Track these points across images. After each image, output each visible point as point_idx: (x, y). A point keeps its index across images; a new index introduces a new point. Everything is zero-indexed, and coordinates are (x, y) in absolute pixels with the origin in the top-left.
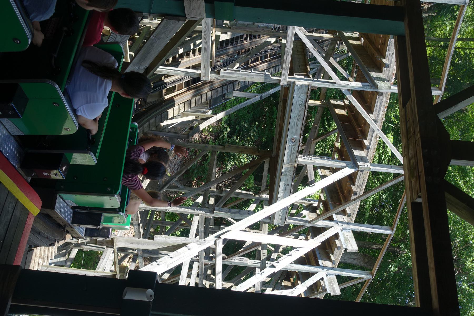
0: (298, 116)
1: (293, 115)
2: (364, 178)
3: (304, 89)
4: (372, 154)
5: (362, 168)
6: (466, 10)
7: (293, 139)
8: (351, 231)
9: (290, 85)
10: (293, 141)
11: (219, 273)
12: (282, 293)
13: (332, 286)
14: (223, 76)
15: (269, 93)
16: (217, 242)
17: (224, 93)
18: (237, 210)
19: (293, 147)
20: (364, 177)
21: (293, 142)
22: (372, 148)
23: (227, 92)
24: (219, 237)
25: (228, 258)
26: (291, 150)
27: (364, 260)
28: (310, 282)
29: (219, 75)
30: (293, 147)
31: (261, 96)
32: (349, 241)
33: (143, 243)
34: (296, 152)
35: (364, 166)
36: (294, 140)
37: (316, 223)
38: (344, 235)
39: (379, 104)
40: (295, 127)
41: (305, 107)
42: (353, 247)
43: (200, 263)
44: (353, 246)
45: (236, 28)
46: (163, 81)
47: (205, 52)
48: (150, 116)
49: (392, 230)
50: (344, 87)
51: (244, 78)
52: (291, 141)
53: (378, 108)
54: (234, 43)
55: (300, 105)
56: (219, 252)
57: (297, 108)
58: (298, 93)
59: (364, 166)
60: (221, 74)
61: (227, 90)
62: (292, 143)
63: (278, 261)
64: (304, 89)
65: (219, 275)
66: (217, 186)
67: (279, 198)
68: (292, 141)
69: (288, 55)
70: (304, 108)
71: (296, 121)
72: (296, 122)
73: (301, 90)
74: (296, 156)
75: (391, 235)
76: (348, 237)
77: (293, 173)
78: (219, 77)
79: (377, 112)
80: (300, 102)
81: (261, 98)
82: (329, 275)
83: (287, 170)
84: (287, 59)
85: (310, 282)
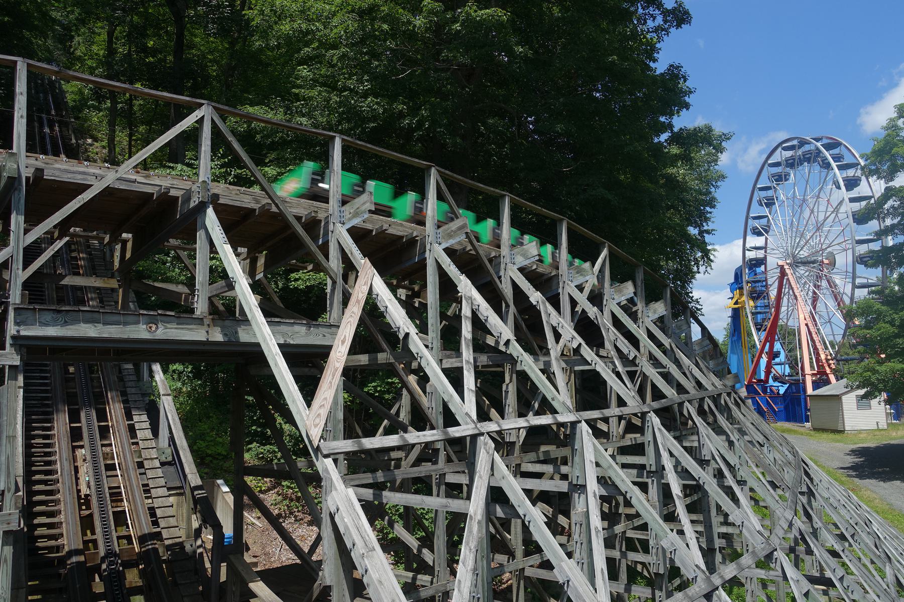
2: (238, 192)
4: (187, 182)
5: (203, 197)
6: (742, 292)
8: (343, 208)
9: (21, 346)
11: (603, 414)
12: (467, 317)
13: (455, 232)
16: (325, 452)
17: (158, 465)
20: (237, 194)
22: (171, 182)
23: (157, 458)
24: (317, 450)
25: (430, 421)
28: (452, 270)
29: (6, 492)
31: (164, 395)
35: (199, 192)
37: (333, 271)
38: (350, 219)
39: (70, 175)
41: (70, 313)
42: (365, 200)
43: (446, 470)
49: (562, 220)
50: (18, 241)
51: (10, 442)
52: (155, 331)
53: (80, 177)
54: (53, 458)
56: (353, 445)
59: (199, 192)
61: (152, 459)
62: (160, 330)
63: (397, 329)
65: (408, 439)
67: (285, 341)
71: (823, 357)
74: (97, 314)
75: (343, 140)
76: (352, 211)
77: (227, 321)
78: (9, 491)
79: (89, 177)
81: (168, 395)
82: (438, 240)
85: (452, 270)
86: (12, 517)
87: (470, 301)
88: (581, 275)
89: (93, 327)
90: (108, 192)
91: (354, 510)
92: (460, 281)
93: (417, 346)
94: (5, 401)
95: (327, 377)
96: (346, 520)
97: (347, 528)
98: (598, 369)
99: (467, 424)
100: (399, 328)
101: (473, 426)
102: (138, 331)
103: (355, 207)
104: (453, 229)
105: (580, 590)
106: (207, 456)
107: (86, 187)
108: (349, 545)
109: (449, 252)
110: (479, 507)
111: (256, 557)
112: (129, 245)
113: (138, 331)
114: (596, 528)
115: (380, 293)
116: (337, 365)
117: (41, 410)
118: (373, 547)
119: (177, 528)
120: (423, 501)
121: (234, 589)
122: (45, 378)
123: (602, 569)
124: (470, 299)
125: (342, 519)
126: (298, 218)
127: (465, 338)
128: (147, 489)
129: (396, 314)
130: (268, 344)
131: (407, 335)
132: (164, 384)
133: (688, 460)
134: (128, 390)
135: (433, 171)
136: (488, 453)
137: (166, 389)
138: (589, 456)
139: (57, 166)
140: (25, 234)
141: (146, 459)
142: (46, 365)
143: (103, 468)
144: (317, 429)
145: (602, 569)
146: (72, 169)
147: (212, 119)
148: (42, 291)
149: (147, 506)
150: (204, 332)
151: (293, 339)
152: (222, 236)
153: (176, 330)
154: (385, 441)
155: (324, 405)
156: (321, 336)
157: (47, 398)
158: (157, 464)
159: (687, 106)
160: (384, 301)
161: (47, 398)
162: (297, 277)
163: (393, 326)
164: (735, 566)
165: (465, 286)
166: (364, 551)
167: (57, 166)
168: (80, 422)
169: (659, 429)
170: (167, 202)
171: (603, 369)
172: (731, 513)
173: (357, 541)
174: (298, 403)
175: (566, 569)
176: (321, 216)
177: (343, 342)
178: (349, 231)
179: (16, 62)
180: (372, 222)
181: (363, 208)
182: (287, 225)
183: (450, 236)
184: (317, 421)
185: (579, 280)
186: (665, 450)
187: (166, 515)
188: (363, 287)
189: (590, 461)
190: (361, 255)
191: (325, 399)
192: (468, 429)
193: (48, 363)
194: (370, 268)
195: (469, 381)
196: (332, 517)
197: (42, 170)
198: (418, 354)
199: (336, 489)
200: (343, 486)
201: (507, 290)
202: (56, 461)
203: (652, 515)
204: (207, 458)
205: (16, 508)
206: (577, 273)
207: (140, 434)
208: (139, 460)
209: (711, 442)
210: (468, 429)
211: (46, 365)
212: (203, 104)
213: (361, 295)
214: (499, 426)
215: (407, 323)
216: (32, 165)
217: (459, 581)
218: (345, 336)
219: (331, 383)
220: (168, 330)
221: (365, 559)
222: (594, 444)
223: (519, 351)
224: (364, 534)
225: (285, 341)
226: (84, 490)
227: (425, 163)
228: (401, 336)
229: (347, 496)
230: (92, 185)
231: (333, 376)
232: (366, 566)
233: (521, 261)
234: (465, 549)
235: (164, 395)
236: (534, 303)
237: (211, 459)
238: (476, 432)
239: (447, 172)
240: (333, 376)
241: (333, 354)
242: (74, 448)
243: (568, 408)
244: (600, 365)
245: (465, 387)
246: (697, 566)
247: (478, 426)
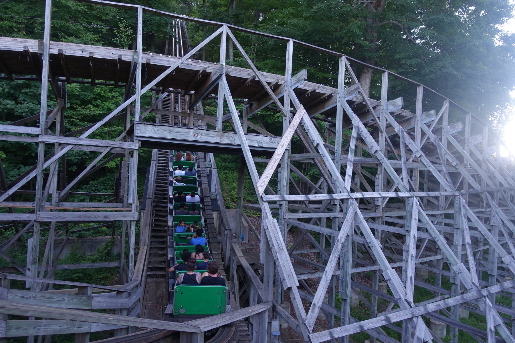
0: (169, 131)
1: (169, 136)
7: (195, 135)
10: (196, 135)
13: (353, 91)
14: (134, 200)
15: (213, 162)
17: (210, 200)
19: (203, 135)
21: (198, 135)
27: (365, 73)
28: (350, 112)
30: (203, 135)
44: (399, 101)
46: (195, 259)
47: (109, 217)
52: (197, 137)
55: (158, 130)
56: (280, 198)
58: (145, 133)
61: (207, 197)
66: (47, 234)
73: (142, 130)
75: (294, 42)
80: (155, 131)
81: (215, 169)
86: (135, 215)
87: (357, 129)
88: (429, 117)
90: (178, 69)
92: (353, 118)
93: (322, 151)
95: (271, 163)
97: (271, 237)
98: (431, 170)
99: (344, 192)
100: (314, 141)
101: (347, 194)
102: (189, 136)
104: (352, 90)
105: (396, 285)
107: (167, 68)
108: (271, 246)
109: (350, 102)
110: (344, 236)
112: (193, 96)
113: (189, 136)
114: (412, 255)
115: (306, 123)
116: (277, 157)
118: (283, 249)
120: (321, 229)
123: (411, 277)
124: (358, 129)
125: (269, 233)
126: (269, 84)
127: (351, 148)
129: (313, 134)
132: (214, 163)
133: (480, 224)
135: (344, 58)
136: (353, 209)
137: (214, 166)
138: (415, 216)
139: (157, 58)
142: (167, 152)
144: (262, 188)
145: (411, 277)
146: (163, 59)
147: (227, 33)
149: (35, 203)
150: (219, 138)
152: (228, 91)
154: (297, 197)
156: (277, 143)
159: (510, 16)
160: (308, 126)
162: (278, 115)
163: (311, 140)
164: (499, 287)
165: (356, 120)
169: (464, 206)
170: (206, 75)
171: (434, 170)
172: (504, 257)
173: (275, 244)
175: (389, 273)
176: (281, 82)
177: (283, 146)
178: (294, 90)
179: (137, 8)
180: (308, 86)
182: (263, 87)
183: (350, 93)
184: (263, 184)
185: (428, 120)
186: (465, 217)
189: (415, 219)
191: (269, 174)
192: (344, 195)
194: (303, 109)
195: (349, 171)
196: (265, 231)
197: (150, 60)
199: (268, 218)
200: (272, 217)
201: (382, 125)
203: (449, 252)
206: (427, 116)
207: (203, 186)
209: (498, 216)
210: (344, 195)
211: (167, 152)
212: (223, 25)
213: (295, 123)
214: (362, 195)
215: (319, 139)
219: (273, 166)
221: (278, 254)
222: (419, 210)
223: (382, 157)
224: (279, 242)
227: (339, 54)
231: (275, 163)
233: (392, 108)
234: (332, 256)
236: (397, 132)
237: (237, 199)
238: (348, 197)
239: (352, 59)
240: (275, 163)
243: (406, 189)
244: (432, 167)
245: (347, 174)
246: (473, 283)
247: (350, 194)
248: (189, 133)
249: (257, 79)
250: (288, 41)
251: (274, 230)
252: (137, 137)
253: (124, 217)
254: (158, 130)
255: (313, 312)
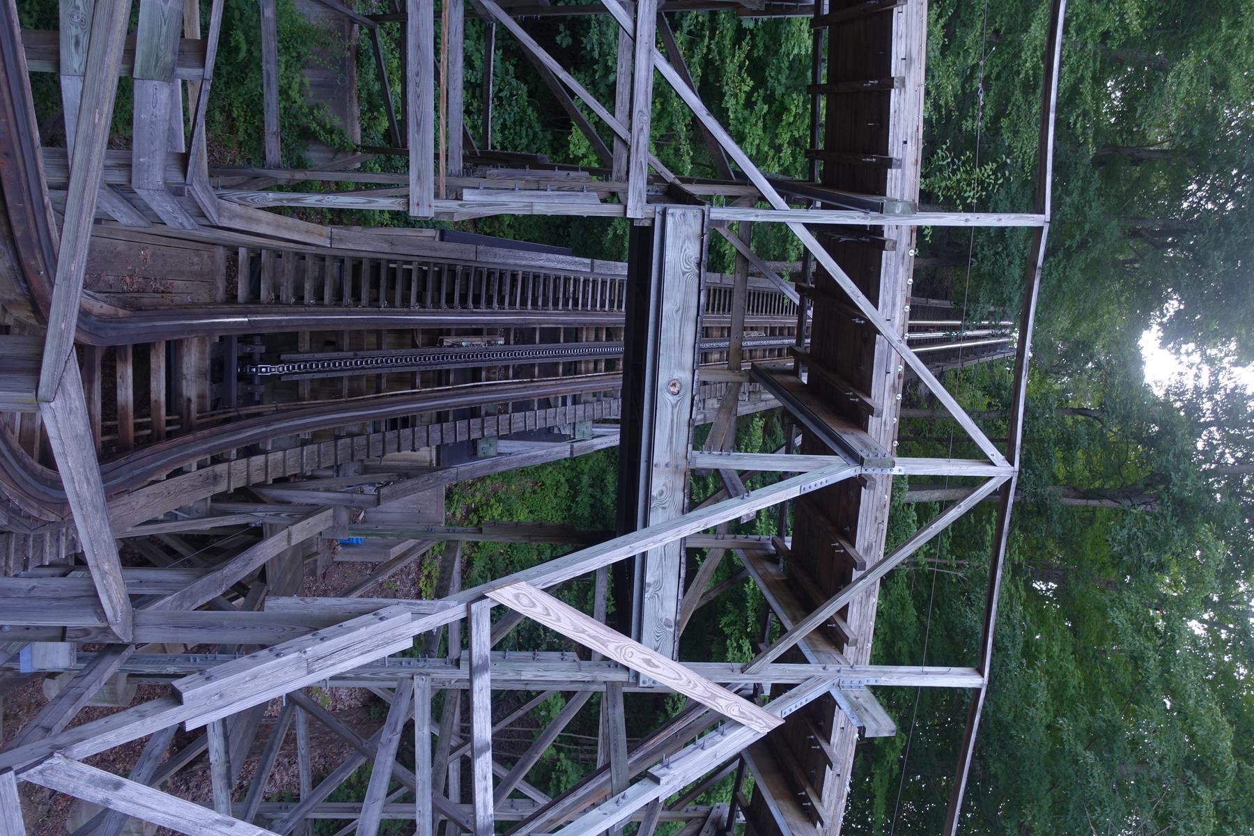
0: (684, 308)
3: (690, 226)
7: (674, 385)
10: (675, 390)
11: (482, 751)
14: (472, 205)
15: (592, 446)
16: (474, 607)
17: (473, 436)
18: (529, 654)
19: (676, 411)
20: (876, 519)
21: (673, 394)
26: (672, 420)
29: (460, 202)
32: (866, 710)
33: (225, 623)
34: (686, 424)
36: (678, 385)
40: (677, 345)
42: (881, 722)
45: (498, 175)
48: (270, 428)
52: (669, 392)
54: (495, 305)
55: (685, 273)
56: (480, 657)
57: (676, 284)
58: (676, 237)
60: (464, 198)
61: (482, 429)
64: (690, 226)
67: (649, 585)
68: (672, 389)
69: (642, 129)
70: (697, 285)
71: (678, 324)
72: (678, 328)
73: (684, 228)
75: (977, 691)
78: (460, 205)
80: (683, 266)
81: (572, 453)
83: (664, 488)
84: (641, 142)
89: (676, 308)
90: (869, 332)
91: (378, 646)
94: (579, 201)
95: (593, 627)
96: (363, 630)
97: (351, 630)
100: (667, 766)
102: (670, 368)
103: (867, 706)
106: (479, 517)
107: (874, 300)
108: (323, 632)
111: (324, 578)
112: (792, 379)
117: (561, 296)
119: (380, 453)
121: (283, 515)
122: (603, 305)
125: (366, 625)
126: (843, 613)
128: (441, 418)
130: (648, 537)
131: (656, 780)
132: (588, 448)
134: (582, 406)
137: (580, 450)
139: (901, 270)
140: (804, 224)
141: (483, 422)
142: (619, 307)
143: (476, 365)
144: (511, 598)
147: (990, 478)
148: (719, 310)
150: (667, 460)
151: (652, 597)
153: (669, 421)
155: (548, 614)
156: (656, 645)
157: (576, 304)
158: (475, 435)
161: (576, 304)
162: (745, 649)
166: (309, 653)
167: (901, 270)
168: (541, 342)
170: (859, 416)
173: (327, 644)
174: (554, 574)
176: (849, 651)
177: (648, 662)
178: (828, 695)
179: (1042, 212)
181: (867, 718)
182: (830, 593)
187: (402, 441)
188: (736, 709)
190: (788, 713)
191: (559, 619)
193: (623, 309)
194: (768, 726)
196: (373, 610)
197: (894, 248)
198: (623, 797)
199: (413, 620)
202: (491, 308)
204: (475, 517)
205: (437, 214)
207: (518, 416)
208: (483, 412)
212: (1012, 464)
213: (723, 703)
215: (676, 782)
216: (900, 235)
217: (231, 825)
218: (657, 667)
219: (583, 632)
220: (670, 409)
221: (296, 655)
224: (336, 657)
225: (649, 585)
226: (448, 341)
228: (655, 771)
229: (401, 637)
230: (877, 307)
232: (285, 655)
235: (572, 447)
241: (629, 642)
242: (506, 332)
248: (680, 366)
249: (856, 574)
250: (981, 673)
251: (376, 640)
252: (664, 214)
253: (419, 177)
254: (684, 273)
255: (93, 781)
